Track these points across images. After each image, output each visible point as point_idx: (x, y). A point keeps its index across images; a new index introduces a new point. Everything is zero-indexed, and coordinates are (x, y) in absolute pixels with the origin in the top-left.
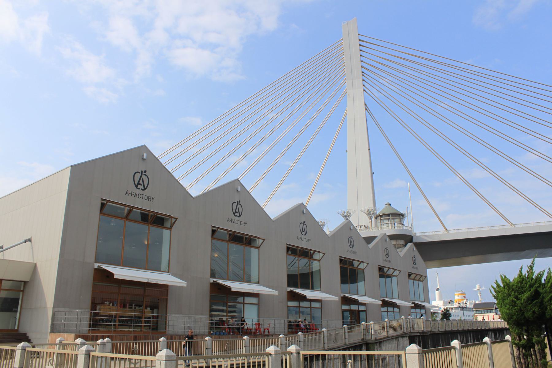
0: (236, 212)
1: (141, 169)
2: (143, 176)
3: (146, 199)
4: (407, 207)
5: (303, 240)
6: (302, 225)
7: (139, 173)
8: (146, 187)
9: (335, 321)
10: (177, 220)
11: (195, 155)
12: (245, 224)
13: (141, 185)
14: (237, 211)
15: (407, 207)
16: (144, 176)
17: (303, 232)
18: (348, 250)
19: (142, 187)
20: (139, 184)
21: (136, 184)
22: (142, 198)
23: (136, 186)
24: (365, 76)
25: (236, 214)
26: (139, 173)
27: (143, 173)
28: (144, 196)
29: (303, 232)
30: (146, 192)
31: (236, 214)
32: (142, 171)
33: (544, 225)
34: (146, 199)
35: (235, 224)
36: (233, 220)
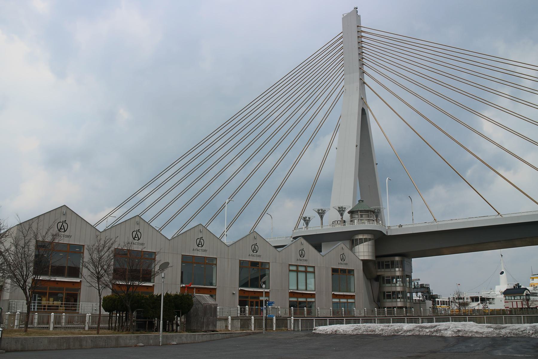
0: (254, 250)
1: (63, 219)
2: (138, 233)
3: (66, 237)
4: (387, 232)
5: (301, 261)
6: (301, 251)
7: (61, 222)
8: (139, 238)
9: (297, 289)
10: (407, 274)
11: (212, 220)
12: (206, 251)
13: (200, 244)
14: (302, 254)
15: (387, 232)
16: (65, 224)
17: (255, 250)
18: (340, 263)
19: (201, 246)
20: (199, 244)
21: (59, 229)
22: (63, 237)
23: (198, 246)
24: (365, 65)
25: (342, 260)
26: (61, 222)
27: (64, 222)
28: (139, 244)
29: (255, 250)
30: (66, 233)
31: (342, 260)
32: (200, 238)
33: (532, 215)
34: (66, 237)
35: (135, 245)
36: (133, 243)
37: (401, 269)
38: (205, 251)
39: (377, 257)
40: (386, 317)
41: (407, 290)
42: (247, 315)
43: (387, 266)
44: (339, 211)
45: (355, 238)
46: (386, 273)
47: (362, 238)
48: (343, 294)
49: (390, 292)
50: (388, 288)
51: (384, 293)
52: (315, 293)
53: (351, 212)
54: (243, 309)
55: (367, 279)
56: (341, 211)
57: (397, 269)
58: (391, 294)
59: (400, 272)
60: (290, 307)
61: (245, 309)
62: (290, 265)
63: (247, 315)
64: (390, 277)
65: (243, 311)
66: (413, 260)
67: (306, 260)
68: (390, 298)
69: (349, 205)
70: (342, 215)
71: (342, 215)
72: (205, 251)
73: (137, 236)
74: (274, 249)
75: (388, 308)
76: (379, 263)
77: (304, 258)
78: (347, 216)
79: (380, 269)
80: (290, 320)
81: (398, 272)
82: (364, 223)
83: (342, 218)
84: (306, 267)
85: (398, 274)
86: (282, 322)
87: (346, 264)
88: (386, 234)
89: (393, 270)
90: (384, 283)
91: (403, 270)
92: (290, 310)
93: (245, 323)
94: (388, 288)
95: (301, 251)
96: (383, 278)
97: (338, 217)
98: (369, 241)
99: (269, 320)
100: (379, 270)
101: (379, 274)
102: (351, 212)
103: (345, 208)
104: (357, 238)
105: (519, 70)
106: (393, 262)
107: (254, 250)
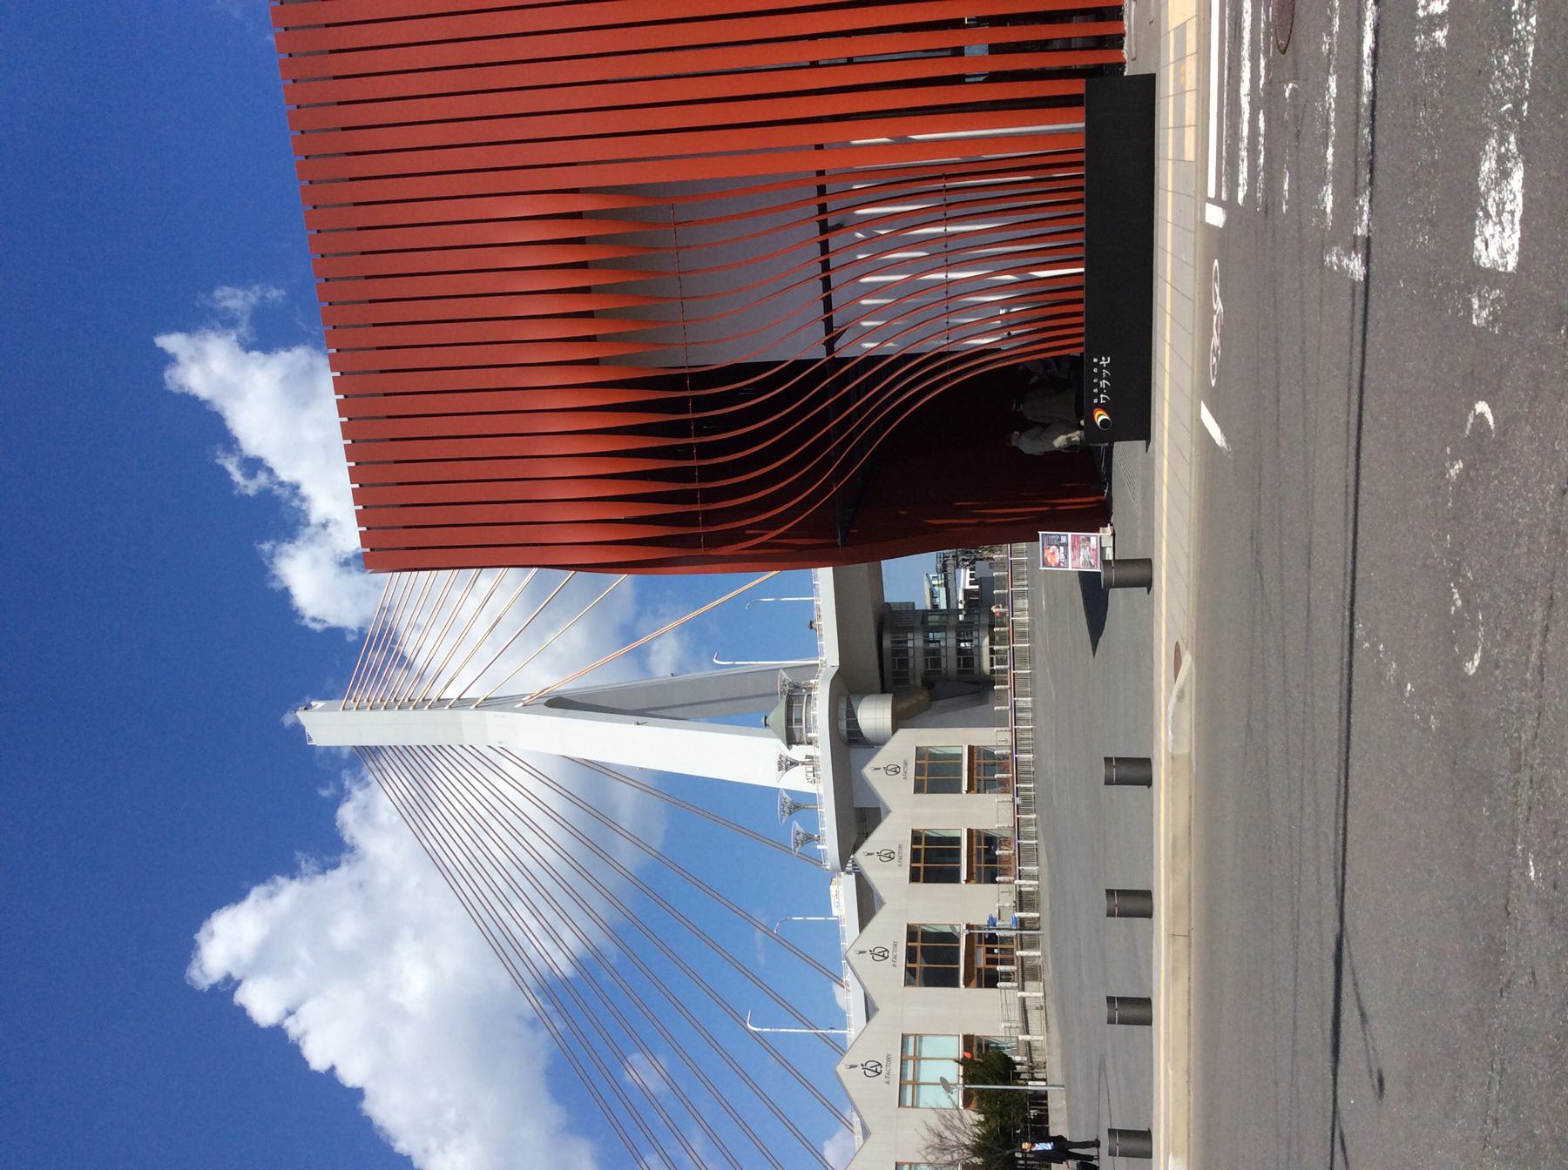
0: (890, 857)
2: (867, 1067)
6: (888, 772)
18: (893, 963)
19: (879, 1067)
20: (883, 956)
23: (886, 958)
37: (910, 636)
38: (888, 1059)
39: (884, 691)
40: (1010, 688)
41: (952, 622)
42: (1014, 968)
43: (904, 663)
44: (787, 769)
45: (846, 735)
46: (917, 664)
47: (845, 721)
48: (966, 772)
49: (959, 660)
50: (950, 664)
51: (960, 672)
52: (966, 830)
53: (791, 740)
54: (1004, 977)
55: (930, 708)
56: (787, 765)
57: (910, 644)
58: (964, 659)
59: (916, 637)
60: (996, 882)
61: (1002, 973)
62: (901, 1103)
63: (1014, 968)
64: (927, 659)
65: (1007, 977)
66: (884, 563)
67: (900, 847)
68: (972, 659)
69: (773, 746)
70: (794, 763)
71: (794, 763)
72: (888, 1059)
73: (874, 1069)
74: (871, 1139)
75: (992, 665)
76: (896, 682)
77: (896, 851)
78: (798, 752)
79: (908, 679)
80: (1020, 886)
81: (915, 642)
82: (815, 716)
83: (803, 764)
84: (903, 1062)
85: (919, 643)
86: (1023, 901)
87: (906, 764)
88: (836, 669)
89: (911, 653)
90: (940, 671)
91: (912, 629)
92: (1000, 882)
93: (1029, 973)
94: (950, 664)
95: (888, 772)
96: (927, 673)
97: (799, 771)
98: (852, 707)
99: (1022, 924)
100: (912, 682)
101: (919, 682)
102: (791, 740)
103: (781, 756)
104: (845, 732)
105: (534, 895)
106: (895, 653)
107: (890, 857)
